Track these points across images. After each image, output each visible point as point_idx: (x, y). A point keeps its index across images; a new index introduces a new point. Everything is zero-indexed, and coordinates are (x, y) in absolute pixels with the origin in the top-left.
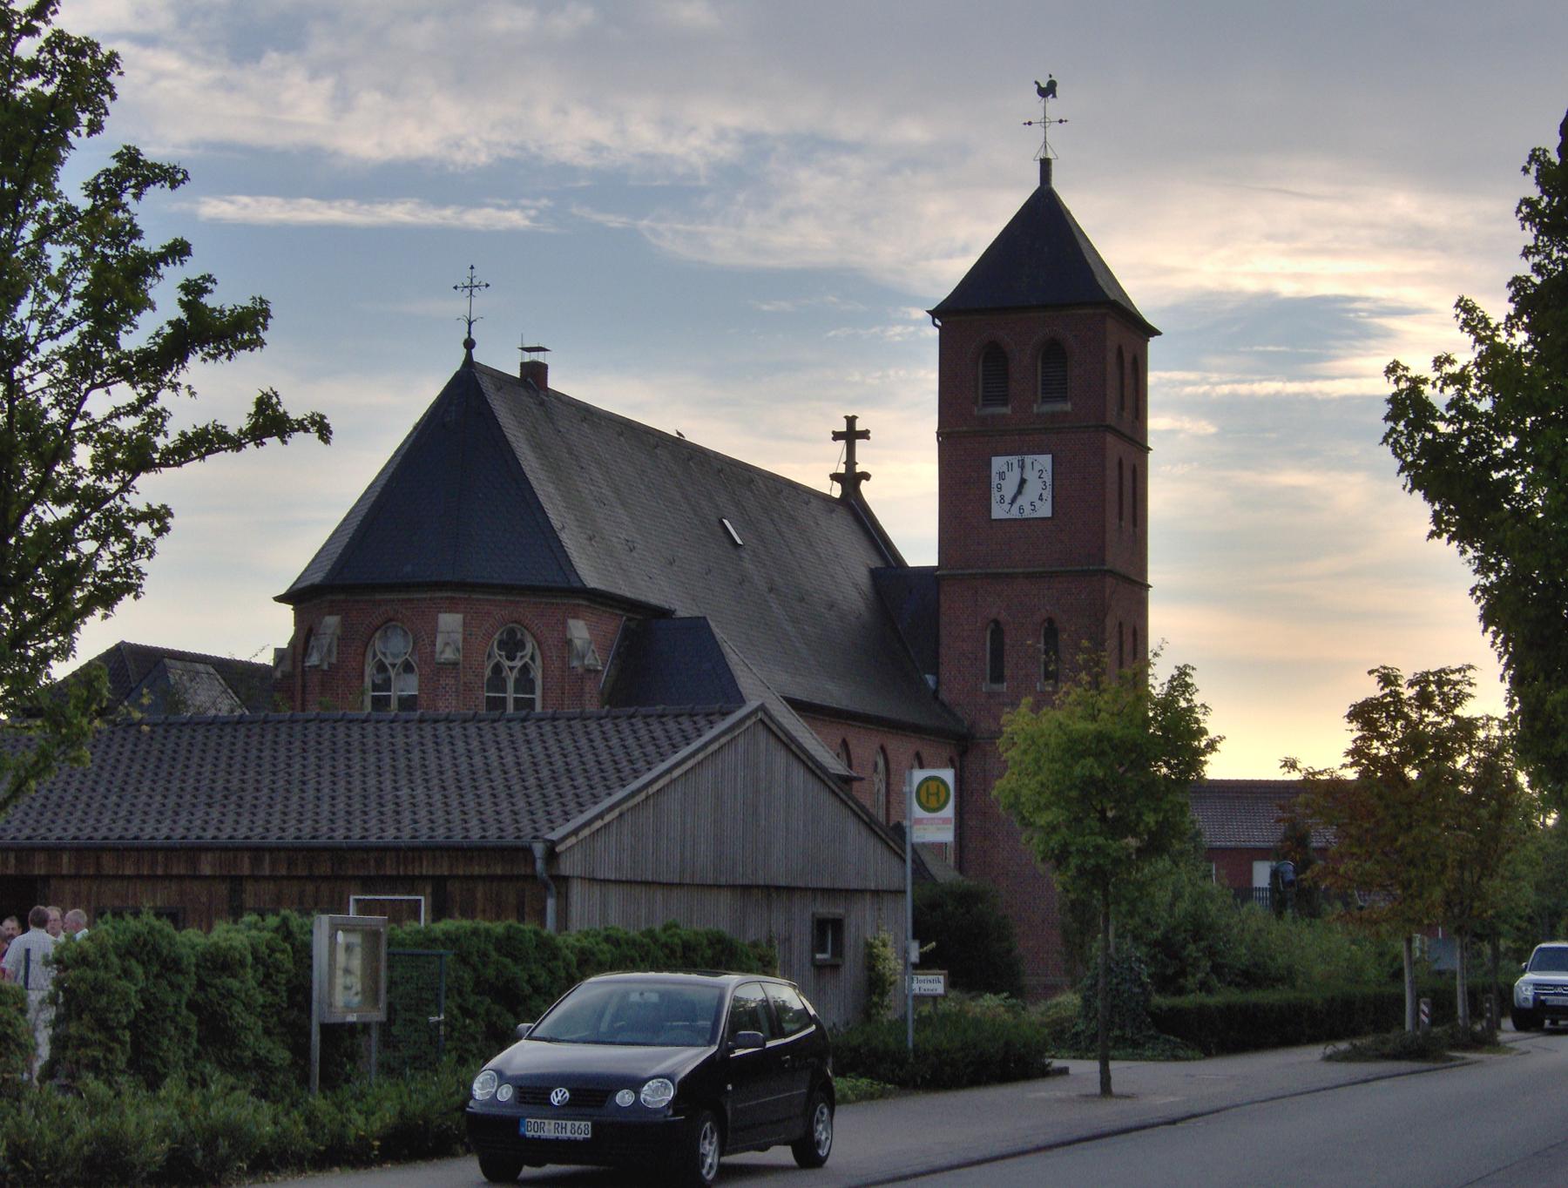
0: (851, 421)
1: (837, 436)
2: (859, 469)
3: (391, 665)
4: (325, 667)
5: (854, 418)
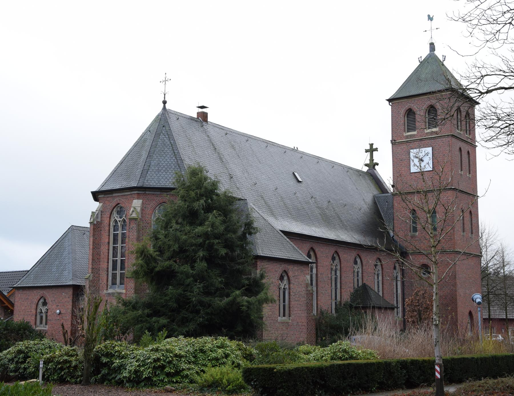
0: (371, 145)
1: (367, 151)
2: (374, 162)
3: (119, 221)
4: (95, 223)
5: (372, 144)
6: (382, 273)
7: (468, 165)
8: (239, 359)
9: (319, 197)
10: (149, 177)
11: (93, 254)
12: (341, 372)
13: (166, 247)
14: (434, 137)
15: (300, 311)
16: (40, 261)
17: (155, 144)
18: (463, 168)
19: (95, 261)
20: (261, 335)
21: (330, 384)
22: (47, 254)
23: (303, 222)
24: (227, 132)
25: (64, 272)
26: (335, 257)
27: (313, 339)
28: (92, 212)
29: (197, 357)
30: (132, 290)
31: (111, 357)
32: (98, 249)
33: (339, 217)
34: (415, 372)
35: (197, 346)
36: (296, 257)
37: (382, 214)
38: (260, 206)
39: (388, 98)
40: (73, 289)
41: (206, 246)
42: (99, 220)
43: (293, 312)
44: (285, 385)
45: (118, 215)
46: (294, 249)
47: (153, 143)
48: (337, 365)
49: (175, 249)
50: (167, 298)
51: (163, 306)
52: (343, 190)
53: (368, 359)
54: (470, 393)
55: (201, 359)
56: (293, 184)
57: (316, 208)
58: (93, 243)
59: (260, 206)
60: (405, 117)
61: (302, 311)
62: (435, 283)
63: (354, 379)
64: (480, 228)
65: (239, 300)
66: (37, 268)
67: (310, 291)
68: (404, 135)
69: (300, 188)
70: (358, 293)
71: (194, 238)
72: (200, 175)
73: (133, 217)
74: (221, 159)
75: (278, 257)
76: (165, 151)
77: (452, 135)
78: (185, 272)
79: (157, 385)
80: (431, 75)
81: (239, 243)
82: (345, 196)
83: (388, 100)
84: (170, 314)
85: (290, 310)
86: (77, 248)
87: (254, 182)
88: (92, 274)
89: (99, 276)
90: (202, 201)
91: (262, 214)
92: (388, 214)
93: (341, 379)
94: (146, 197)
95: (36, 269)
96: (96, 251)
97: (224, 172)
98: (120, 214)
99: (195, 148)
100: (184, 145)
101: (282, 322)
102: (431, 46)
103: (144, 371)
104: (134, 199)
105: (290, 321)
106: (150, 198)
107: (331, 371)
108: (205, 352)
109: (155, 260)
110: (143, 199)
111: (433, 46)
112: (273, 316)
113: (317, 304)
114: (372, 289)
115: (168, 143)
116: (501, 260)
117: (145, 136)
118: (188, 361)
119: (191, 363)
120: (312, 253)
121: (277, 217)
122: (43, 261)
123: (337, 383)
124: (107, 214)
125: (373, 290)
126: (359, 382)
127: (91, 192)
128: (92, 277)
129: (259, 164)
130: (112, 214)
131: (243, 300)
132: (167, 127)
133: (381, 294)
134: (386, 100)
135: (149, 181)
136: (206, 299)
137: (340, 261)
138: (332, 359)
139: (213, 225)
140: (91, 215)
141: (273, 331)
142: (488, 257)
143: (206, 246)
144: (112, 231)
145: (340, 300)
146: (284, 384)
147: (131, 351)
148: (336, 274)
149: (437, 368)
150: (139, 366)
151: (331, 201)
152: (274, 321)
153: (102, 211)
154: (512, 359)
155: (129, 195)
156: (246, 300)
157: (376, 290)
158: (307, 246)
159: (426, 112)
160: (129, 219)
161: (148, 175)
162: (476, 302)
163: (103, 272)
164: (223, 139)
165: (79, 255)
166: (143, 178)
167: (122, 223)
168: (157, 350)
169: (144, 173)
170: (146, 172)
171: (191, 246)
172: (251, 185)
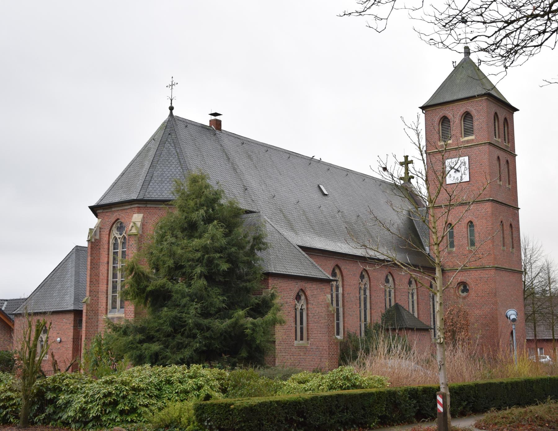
4: (93, 240)
5: (407, 156)
6: (417, 292)
7: (507, 175)
8: (215, 390)
9: (347, 212)
10: (151, 189)
11: (90, 275)
12: (327, 406)
13: (161, 263)
14: (470, 146)
15: (320, 333)
16: (41, 285)
17: (159, 153)
18: (502, 178)
19: (94, 283)
20: (273, 361)
21: (312, 421)
22: (49, 277)
23: (327, 237)
24: (243, 141)
25: (65, 296)
26: (363, 276)
27: (335, 364)
28: (90, 229)
29: (162, 389)
30: (132, 314)
31: (58, 392)
32: (97, 269)
33: (368, 232)
34: (428, 402)
35: (163, 377)
36: (315, 274)
37: (418, 230)
38: (279, 220)
39: (421, 106)
40: (74, 315)
41: (205, 261)
42: (98, 237)
43: (311, 335)
44: (244, 426)
45: (118, 231)
46: (313, 265)
47: (157, 152)
48: (321, 397)
49: (170, 265)
50: (161, 321)
51: (158, 331)
52: (374, 204)
53: (375, 387)
54: (491, 426)
55: (167, 392)
56: (317, 197)
57: (343, 223)
58: (91, 263)
59: (279, 220)
60: (439, 125)
61: (323, 333)
62: (438, 291)
63: (346, 414)
64: (522, 245)
65: (242, 321)
66: (39, 293)
67: (331, 311)
68: (439, 144)
69: (325, 201)
70: (390, 313)
71: (191, 253)
72: (200, 182)
73: (132, 233)
74: (235, 169)
75: (293, 274)
76: (169, 161)
77: (489, 143)
78: (180, 290)
79: (107, 425)
80: (466, 80)
81: (245, 258)
82: (376, 211)
83: (420, 108)
84: (164, 339)
85: (308, 335)
86: (81, 270)
87: (273, 194)
88: (90, 298)
89: (98, 300)
90: (202, 212)
91: (278, 229)
92: (424, 229)
93: (328, 415)
94: (147, 211)
95: (37, 293)
96: (95, 272)
97: (237, 183)
98: (120, 231)
99: (205, 157)
100: (192, 153)
101: (299, 347)
102: (466, 50)
103: (92, 408)
104: (134, 214)
105: (309, 346)
106: (152, 211)
107: (313, 405)
108: (173, 383)
109: (148, 278)
110: (144, 213)
111: (468, 50)
112: (288, 340)
113: (344, 326)
114: (405, 310)
115: (174, 152)
116: (546, 277)
117: (149, 145)
118: (148, 395)
119: (153, 397)
120: (337, 271)
121: (298, 232)
122: (45, 285)
123: (321, 419)
124: (106, 231)
125: (406, 310)
126: (352, 417)
127: (89, 207)
128: (90, 301)
129: (279, 175)
130: (112, 231)
131: (247, 322)
132: (174, 135)
133: (416, 315)
134: (419, 107)
135: (151, 193)
136: (204, 321)
137: (370, 280)
138: (331, 388)
139: (213, 238)
140: (89, 233)
141: (288, 357)
142: (533, 274)
143: (205, 261)
144: (111, 250)
145: (370, 322)
146: (243, 425)
147: (84, 383)
148: (365, 294)
149: (439, 399)
150: (86, 403)
151: (361, 215)
152: (289, 345)
153: (100, 228)
154: (549, 383)
155: (129, 209)
156: (251, 322)
157: (411, 311)
158: (331, 264)
159: (461, 119)
160: (128, 235)
161: (149, 186)
162: (510, 319)
163: (102, 295)
164: (238, 149)
165: (82, 277)
166: (144, 190)
167: (123, 240)
168: (110, 382)
169: (146, 184)
170: (147, 183)
171: (188, 261)
172: (269, 197)
